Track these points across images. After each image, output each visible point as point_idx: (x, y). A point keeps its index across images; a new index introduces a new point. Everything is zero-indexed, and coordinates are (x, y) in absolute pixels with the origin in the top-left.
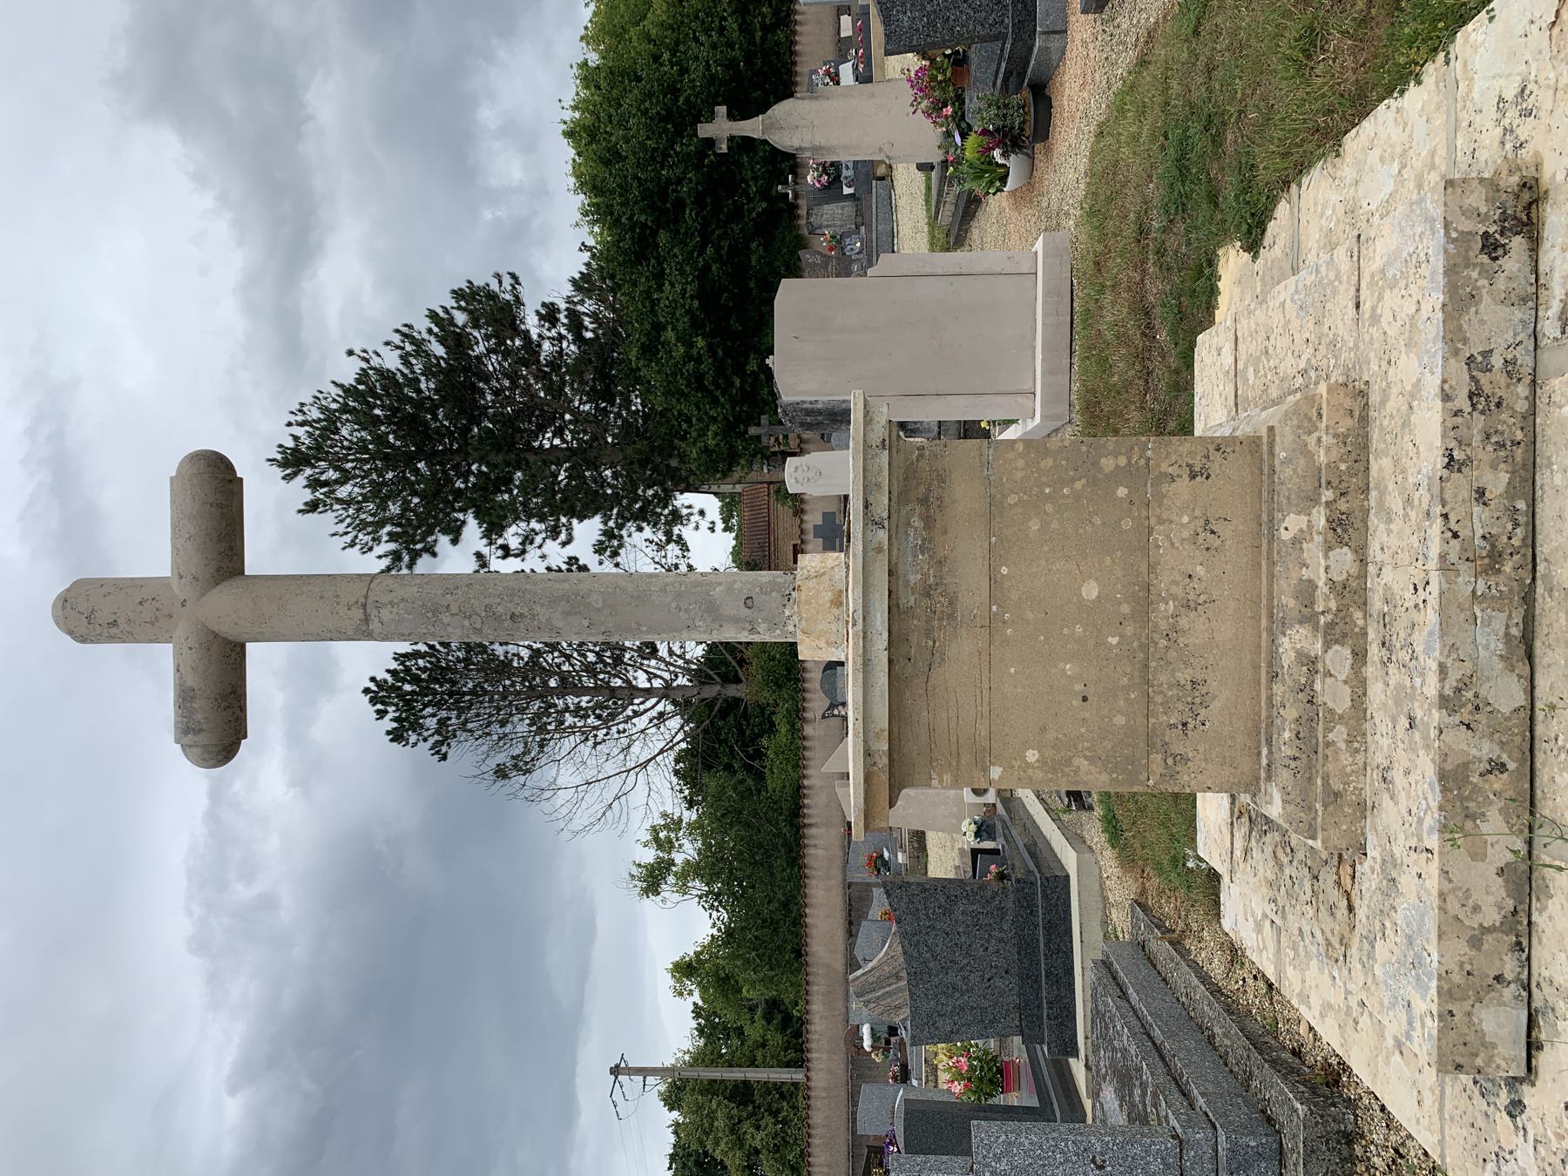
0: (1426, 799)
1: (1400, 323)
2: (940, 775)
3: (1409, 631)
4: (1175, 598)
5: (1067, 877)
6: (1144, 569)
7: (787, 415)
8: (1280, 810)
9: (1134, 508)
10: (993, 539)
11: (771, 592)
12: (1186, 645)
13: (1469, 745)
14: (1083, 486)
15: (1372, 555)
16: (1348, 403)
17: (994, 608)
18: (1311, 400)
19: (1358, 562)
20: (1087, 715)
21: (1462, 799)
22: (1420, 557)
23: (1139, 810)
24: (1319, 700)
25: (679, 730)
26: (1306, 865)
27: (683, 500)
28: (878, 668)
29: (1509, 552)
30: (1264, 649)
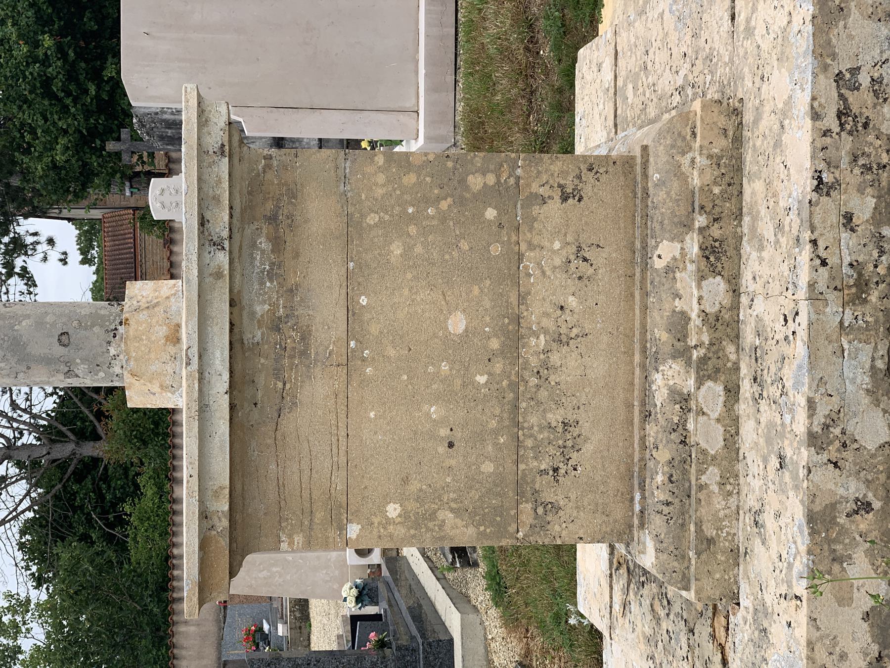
0: (795, 542)
1: (772, 35)
2: (290, 536)
3: (779, 364)
4: (546, 332)
5: (451, 641)
6: (514, 299)
7: (144, 126)
8: (653, 559)
9: (504, 232)
10: (351, 265)
11: (93, 326)
12: (558, 384)
13: (836, 484)
14: (449, 206)
15: (744, 285)
16: (722, 121)
17: (352, 344)
18: (685, 117)
19: (731, 293)
20: (453, 462)
21: (829, 541)
22: (790, 286)
23: (523, 564)
24: (692, 440)
25: (25, 497)
26: (682, 617)
27: (26, 226)
28: (218, 414)
29: (875, 280)
30: (637, 387)
